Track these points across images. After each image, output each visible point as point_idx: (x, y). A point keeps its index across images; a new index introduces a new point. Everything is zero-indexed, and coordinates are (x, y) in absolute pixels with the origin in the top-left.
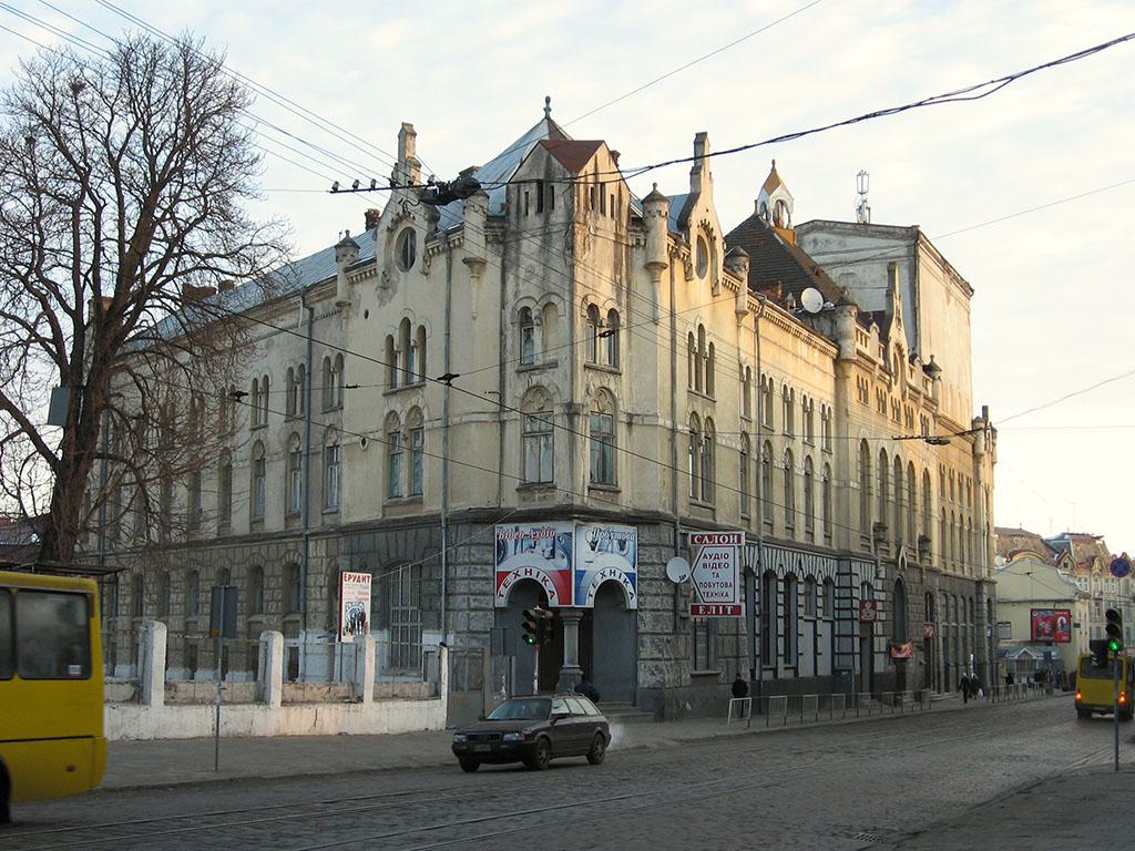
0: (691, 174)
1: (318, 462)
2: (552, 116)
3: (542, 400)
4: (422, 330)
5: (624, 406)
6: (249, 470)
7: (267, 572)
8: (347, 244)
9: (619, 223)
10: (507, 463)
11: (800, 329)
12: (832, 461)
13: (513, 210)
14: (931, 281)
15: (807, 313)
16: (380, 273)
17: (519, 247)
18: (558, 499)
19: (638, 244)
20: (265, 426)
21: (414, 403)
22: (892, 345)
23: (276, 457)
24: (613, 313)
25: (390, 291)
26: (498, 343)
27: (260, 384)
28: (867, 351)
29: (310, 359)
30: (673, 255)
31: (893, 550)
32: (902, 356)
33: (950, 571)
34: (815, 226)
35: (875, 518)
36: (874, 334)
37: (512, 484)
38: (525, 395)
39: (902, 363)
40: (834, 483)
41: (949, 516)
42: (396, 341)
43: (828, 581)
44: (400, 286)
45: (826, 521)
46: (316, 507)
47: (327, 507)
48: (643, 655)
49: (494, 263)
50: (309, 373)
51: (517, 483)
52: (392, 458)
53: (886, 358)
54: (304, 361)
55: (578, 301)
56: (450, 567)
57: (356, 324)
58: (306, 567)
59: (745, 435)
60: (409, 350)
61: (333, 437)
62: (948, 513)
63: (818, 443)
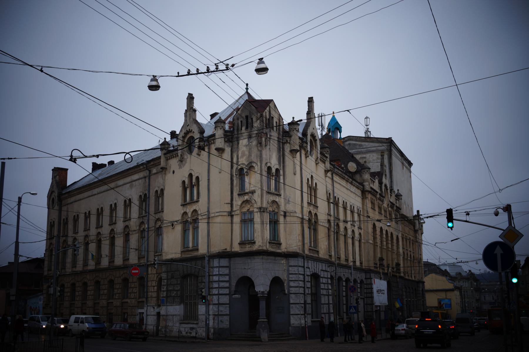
0: (307, 114)
1: (152, 235)
2: (249, 91)
3: (249, 206)
4: (197, 178)
5: (282, 208)
6: (122, 238)
7: (130, 280)
8: (164, 145)
9: (279, 134)
10: (234, 233)
11: (349, 178)
12: (362, 232)
13: (236, 128)
14: (396, 162)
15: (350, 172)
16: (179, 155)
17: (238, 143)
18: (255, 248)
19: (287, 142)
20: (89, 230)
21: (185, 211)
22: (383, 185)
23: (134, 232)
24: (277, 170)
25: (184, 162)
26: (230, 183)
27: (113, 206)
28: (374, 188)
29: (149, 191)
30: (301, 147)
31: (386, 269)
32: (387, 189)
33: (407, 277)
34: (350, 138)
35: (379, 255)
36: (377, 181)
37: (237, 239)
38: (242, 204)
39: (387, 192)
40: (363, 241)
41: (406, 255)
42: (187, 183)
43: (362, 282)
44: (188, 160)
45: (360, 255)
46: (152, 254)
47: (156, 252)
48: (292, 313)
49: (228, 150)
50: (149, 197)
51: (239, 241)
52: (185, 231)
53: (381, 190)
54: (147, 192)
55: (263, 165)
56: (211, 277)
57: (169, 176)
58: (147, 278)
59: (329, 221)
60: (192, 187)
61: (159, 223)
62: (406, 253)
63: (357, 224)
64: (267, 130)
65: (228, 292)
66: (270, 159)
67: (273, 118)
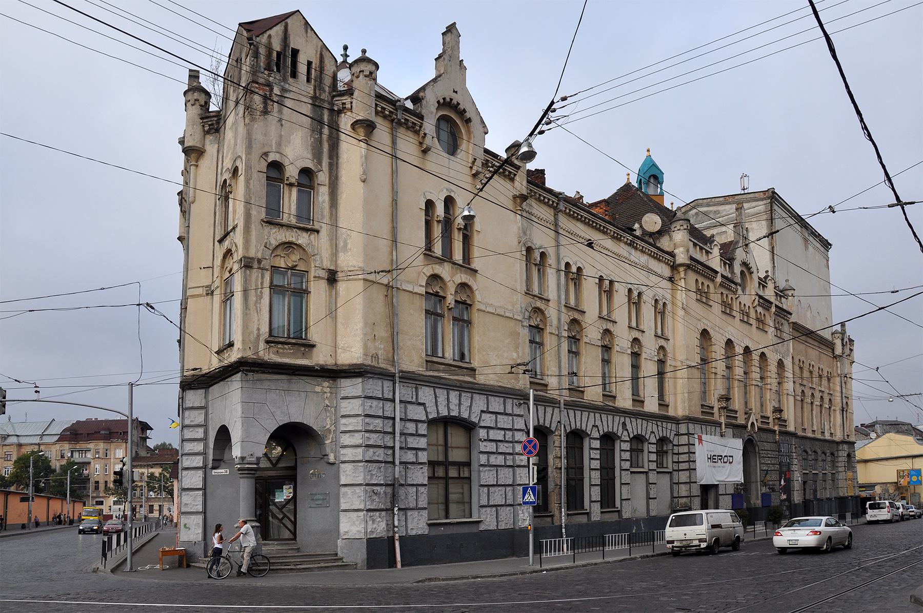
64: (274, 78)
65: (201, 464)
66: (279, 144)
67: (295, 53)
